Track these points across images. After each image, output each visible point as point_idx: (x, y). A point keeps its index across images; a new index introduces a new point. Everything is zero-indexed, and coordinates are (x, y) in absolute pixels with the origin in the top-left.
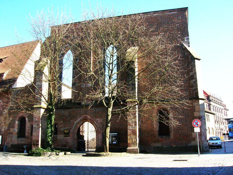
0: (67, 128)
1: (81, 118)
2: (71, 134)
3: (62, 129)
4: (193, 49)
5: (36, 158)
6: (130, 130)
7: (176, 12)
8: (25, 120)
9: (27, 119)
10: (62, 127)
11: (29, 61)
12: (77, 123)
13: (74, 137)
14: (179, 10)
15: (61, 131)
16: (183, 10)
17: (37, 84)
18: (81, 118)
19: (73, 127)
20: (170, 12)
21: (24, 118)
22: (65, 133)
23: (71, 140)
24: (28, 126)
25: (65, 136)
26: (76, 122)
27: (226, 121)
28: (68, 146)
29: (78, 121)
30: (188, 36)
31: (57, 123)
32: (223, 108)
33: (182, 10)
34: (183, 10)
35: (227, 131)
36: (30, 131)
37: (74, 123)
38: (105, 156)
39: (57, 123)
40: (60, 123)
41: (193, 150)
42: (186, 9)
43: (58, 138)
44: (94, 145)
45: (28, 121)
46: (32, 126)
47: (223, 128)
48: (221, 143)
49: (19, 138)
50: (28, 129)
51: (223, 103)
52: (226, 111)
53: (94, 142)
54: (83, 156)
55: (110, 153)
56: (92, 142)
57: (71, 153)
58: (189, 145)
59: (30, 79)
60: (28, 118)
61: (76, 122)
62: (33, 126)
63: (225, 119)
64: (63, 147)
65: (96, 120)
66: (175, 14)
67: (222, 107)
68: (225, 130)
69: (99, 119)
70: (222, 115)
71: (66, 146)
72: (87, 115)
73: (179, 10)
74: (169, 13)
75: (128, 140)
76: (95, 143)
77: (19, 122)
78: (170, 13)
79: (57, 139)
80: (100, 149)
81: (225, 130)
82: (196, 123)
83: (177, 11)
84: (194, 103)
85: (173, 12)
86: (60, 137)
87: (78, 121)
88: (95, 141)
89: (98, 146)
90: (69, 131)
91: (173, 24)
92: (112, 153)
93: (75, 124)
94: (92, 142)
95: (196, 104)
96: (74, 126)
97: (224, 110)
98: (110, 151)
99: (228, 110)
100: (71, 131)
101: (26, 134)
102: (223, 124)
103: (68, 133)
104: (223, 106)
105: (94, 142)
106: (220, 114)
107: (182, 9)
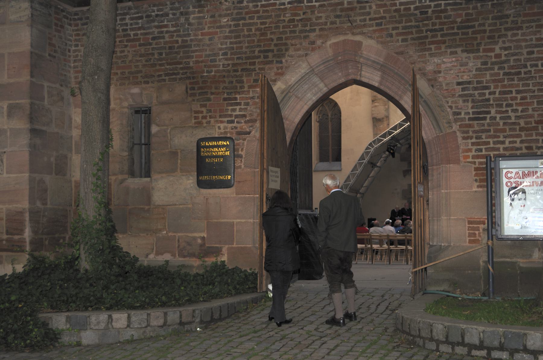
15: (174, 154)
25: (201, 184)
28: (225, 250)
43: (159, 197)
64: (192, 255)
65: (430, 68)
72: (358, 38)
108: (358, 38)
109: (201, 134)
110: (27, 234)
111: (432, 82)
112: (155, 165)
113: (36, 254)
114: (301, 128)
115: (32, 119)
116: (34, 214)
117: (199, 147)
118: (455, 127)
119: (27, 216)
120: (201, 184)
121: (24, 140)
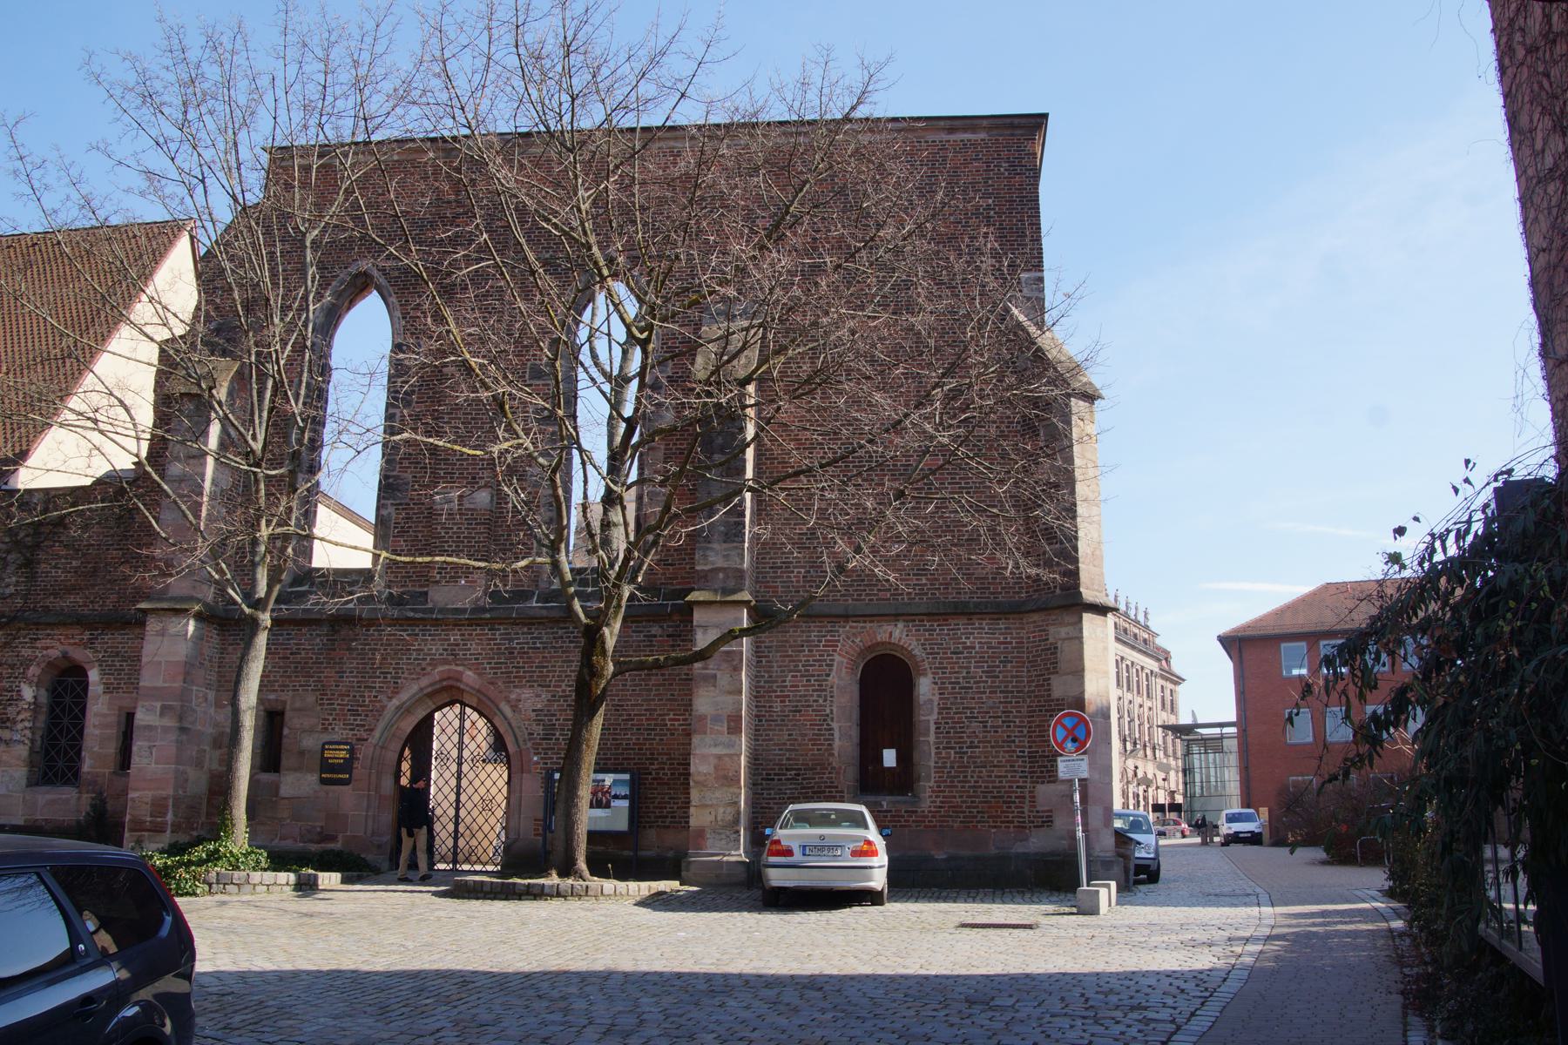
0: (336, 738)
1: (424, 682)
2: (359, 770)
3: (310, 742)
4: (1069, 334)
5: (762, 964)
6: (704, 757)
7: (982, 135)
8: (84, 685)
9: (94, 675)
10: (311, 731)
11: (123, 340)
12: (398, 708)
13: (378, 787)
14: (997, 127)
15: (302, 753)
16: (1019, 127)
17: (176, 468)
18: (424, 682)
19: (377, 734)
20: (951, 130)
21: (79, 672)
22: (326, 766)
23: (361, 810)
24: (105, 716)
25: (323, 782)
26: (396, 702)
27: (1170, 737)
28: (340, 836)
29: (404, 696)
30: (1039, 266)
31: (284, 703)
32: (1156, 670)
33: (1012, 126)
34: (1019, 127)
35: (1172, 793)
36: (112, 749)
37: (384, 707)
38: (565, 897)
39: (284, 703)
40: (298, 705)
41: (1052, 878)
42: (1035, 124)
43: (285, 791)
44: (492, 836)
45: (101, 688)
46: (123, 719)
47: (1150, 776)
48: (1157, 851)
49: (37, 784)
50: (97, 732)
51: (1159, 641)
52: (1169, 686)
53: (492, 821)
54: (657, 902)
55: (596, 882)
56: (480, 820)
57: (344, 881)
58: (1019, 848)
59: (131, 444)
60: (103, 673)
61: (396, 702)
62: (130, 716)
63: (1165, 727)
64: (311, 841)
65: (513, 696)
66: (974, 144)
67: (1152, 665)
68: (1160, 783)
69: (527, 693)
70: (1148, 704)
71: (333, 839)
72: (460, 668)
73: (997, 127)
74: (945, 137)
75: (692, 810)
76: (498, 828)
77: (43, 692)
78: (952, 137)
79: (277, 794)
80: (531, 862)
81: (1160, 783)
82: (1074, 728)
83: (989, 129)
84: (1052, 630)
85: (965, 130)
86: (297, 784)
87: (404, 696)
88: (500, 813)
89: (516, 840)
90: (352, 751)
91: (990, 170)
92: (609, 885)
93: (388, 714)
94: (480, 820)
95: (1064, 631)
96: (381, 725)
97: (1160, 682)
98: (598, 869)
99: (1178, 680)
100: (364, 752)
101: (86, 767)
102: (1149, 752)
103: (347, 766)
104: (1158, 660)
105: (492, 821)
106: (1138, 700)
107: (1016, 121)
108: (460, 668)
109: (326, 737)
110: (170, 817)
111: (515, 708)
112: (285, 762)
113: (483, 870)
114: (846, 617)
115: (181, 719)
116: (176, 800)
117: (323, 749)
118: (529, 744)
119: (171, 802)
120: (323, 782)
121: (173, 737)
